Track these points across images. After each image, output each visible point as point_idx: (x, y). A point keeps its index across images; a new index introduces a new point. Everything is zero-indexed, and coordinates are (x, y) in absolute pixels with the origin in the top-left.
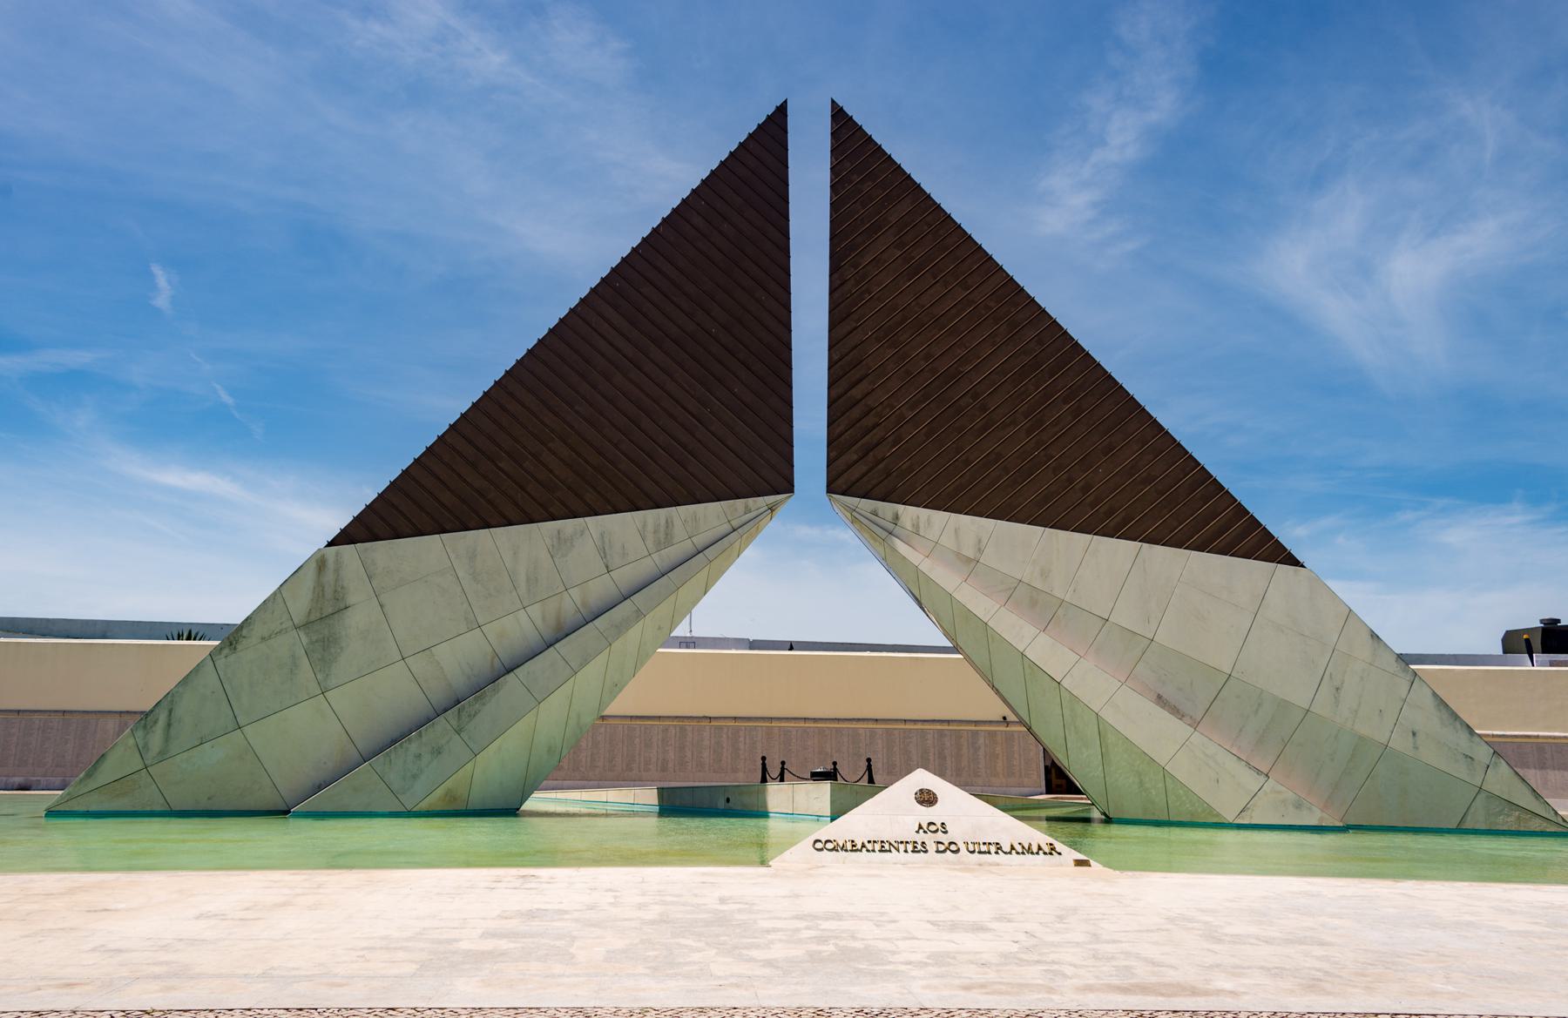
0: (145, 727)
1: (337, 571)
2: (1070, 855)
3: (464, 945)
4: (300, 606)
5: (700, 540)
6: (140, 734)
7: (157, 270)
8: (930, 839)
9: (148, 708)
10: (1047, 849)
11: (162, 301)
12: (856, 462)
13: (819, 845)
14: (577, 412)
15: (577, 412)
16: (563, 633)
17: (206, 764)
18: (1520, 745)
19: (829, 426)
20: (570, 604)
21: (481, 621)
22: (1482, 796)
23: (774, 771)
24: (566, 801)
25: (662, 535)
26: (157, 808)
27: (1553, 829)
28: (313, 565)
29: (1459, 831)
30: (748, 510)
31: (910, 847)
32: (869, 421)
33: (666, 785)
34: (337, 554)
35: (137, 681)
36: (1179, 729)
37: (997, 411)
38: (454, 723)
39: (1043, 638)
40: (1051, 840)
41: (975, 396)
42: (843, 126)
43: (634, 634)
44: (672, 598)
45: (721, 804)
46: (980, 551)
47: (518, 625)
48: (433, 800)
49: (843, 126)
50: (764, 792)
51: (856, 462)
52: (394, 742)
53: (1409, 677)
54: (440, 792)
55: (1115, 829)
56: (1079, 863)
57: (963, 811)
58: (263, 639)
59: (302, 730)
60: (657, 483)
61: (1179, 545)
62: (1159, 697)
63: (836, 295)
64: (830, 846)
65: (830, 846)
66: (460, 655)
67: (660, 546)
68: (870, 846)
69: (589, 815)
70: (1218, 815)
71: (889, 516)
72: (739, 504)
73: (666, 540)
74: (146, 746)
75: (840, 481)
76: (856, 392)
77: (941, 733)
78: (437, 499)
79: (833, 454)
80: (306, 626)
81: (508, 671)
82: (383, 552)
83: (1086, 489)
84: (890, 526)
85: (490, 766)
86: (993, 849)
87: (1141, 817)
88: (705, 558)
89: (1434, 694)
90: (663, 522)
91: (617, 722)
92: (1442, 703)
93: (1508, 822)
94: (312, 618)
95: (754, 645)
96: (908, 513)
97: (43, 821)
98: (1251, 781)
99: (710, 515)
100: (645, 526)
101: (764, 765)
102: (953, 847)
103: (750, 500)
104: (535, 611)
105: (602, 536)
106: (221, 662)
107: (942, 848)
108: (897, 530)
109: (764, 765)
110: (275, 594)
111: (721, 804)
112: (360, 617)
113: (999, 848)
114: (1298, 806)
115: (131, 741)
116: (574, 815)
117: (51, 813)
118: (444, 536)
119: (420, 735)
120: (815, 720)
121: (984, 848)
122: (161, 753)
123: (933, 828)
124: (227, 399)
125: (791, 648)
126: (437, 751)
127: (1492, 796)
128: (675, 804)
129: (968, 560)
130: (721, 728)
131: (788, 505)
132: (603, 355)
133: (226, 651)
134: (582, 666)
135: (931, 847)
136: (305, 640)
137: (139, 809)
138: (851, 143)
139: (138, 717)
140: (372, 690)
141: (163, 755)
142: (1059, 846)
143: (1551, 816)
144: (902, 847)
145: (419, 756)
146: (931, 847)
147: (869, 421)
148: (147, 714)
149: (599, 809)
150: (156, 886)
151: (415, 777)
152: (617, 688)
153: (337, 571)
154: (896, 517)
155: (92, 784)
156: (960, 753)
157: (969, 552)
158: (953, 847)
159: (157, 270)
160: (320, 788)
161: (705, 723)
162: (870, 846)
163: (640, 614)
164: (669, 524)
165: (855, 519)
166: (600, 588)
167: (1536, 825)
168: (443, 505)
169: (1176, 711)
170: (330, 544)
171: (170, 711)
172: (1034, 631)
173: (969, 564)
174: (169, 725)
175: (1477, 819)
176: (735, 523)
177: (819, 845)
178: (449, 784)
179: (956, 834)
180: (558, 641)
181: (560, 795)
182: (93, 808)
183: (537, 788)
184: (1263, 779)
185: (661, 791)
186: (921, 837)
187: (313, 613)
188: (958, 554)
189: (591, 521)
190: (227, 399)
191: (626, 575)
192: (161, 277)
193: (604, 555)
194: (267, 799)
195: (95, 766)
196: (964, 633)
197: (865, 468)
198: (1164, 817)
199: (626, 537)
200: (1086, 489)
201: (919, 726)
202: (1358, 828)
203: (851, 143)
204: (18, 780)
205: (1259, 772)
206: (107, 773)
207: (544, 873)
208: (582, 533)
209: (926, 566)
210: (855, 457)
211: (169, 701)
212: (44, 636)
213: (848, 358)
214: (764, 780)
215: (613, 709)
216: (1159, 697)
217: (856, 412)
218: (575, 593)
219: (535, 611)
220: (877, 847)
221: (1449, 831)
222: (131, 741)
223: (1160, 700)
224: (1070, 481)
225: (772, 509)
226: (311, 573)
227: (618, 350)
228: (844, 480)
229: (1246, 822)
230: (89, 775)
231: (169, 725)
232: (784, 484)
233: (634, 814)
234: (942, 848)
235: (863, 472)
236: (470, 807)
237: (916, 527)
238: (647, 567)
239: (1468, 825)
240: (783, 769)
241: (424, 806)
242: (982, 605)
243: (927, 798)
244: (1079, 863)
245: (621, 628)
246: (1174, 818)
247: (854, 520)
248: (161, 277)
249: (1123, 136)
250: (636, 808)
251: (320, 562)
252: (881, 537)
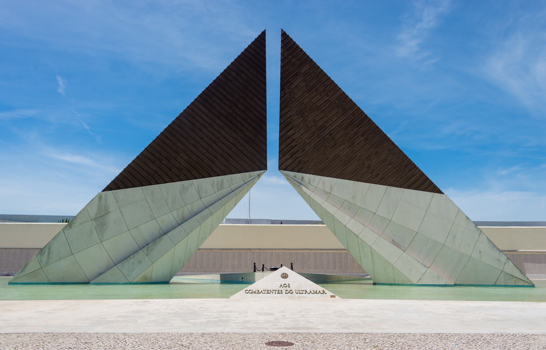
0: (41, 254)
1: (106, 200)
2: (329, 294)
3: (108, 319)
4: (93, 213)
5: (233, 187)
6: (39, 256)
7: (58, 78)
8: (284, 289)
9: (43, 247)
10: (322, 292)
11: (61, 90)
12: (288, 159)
13: (247, 292)
14: (189, 143)
15: (189, 143)
16: (184, 220)
17: (61, 267)
18: (533, 255)
19: (279, 146)
20: (187, 211)
21: (156, 216)
22: (503, 273)
23: (259, 267)
24: (190, 279)
25: (220, 186)
26: (45, 282)
27: (527, 284)
28: (97, 198)
29: (495, 285)
30: (250, 176)
31: (277, 292)
32: (294, 144)
33: (222, 273)
34: (106, 194)
35: (37, 237)
36: (399, 251)
37: (340, 139)
38: (146, 252)
39: (353, 220)
40: (323, 289)
41: (331, 135)
42: (286, 39)
43: (209, 220)
44: (223, 207)
45: (240, 280)
46: (332, 190)
47: (168, 218)
48: (139, 279)
49: (286, 39)
50: (254, 275)
51: (288, 159)
52: (126, 259)
53: (479, 232)
54: (141, 276)
55: (377, 287)
56: (332, 296)
57: (296, 280)
58: (81, 224)
59: (93, 257)
60: (218, 167)
61: (401, 187)
62: (393, 240)
63: (282, 99)
64: (250, 292)
65: (250, 292)
66: (148, 229)
67: (219, 190)
68: (264, 292)
69: (199, 284)
70: (411, 282)
71: (300, 178)
72: (247, 174)
73: (222, 187)
74: (41, 261)
75: (283, 166)
76: (289, 134)
77: (334, 254)
78: (140, 174)
79: (281, 156)
80: (95, 219)
81: (165, 234)
82: (122, 193)
83: (369, 167)
84: (300, 181)
85: (158, 268)
86: (304, 292)
87: (385, 282)
88: (236, 193)
89: (488, 238)
90: (220, 181)
91: (217, 251)
92: (490, 241)
93: (511, 282)
94: (97, 216)
95: (273, 222)
96: (307, 177)
97: (8, 286)
98: (423, 270)
99: (237, 178)
100: (213, 182)
101: (255, 266)
102: (291, 292)
103: (251, 173)
104: (175, 213)
105: (198, 186)
106: (66, 232)
107: (287, 292)
108: (303, 183)
109: (255, 266)
110: (84, 208)
111: (240, 280)
112: (114, 216)
113: (306, 292)
114: (438, 278)
115: (36, 259)
116: (196, 284)
117: (10, 283)
118: (143, 187)
119: (134, 256)
120: (288, 249)
121: (301, 292)
122: (46, 263)
123: (285, 286)
124: (87, 127)
125: (281, 223)
126: (140, 262)
127: (506, 273)
128: (226, 280)
129: (327, 193)
130: (254, 253)
131: (267, 172)
132: (199, 122)
133: (68, 228)
134: (191, 232)
135: (284, 292)
136: (95, 224)
137: (39, 282)
138: (288, 45)
139: (37, 252)
140: (119, 242)
141: (47, 264)
142: (326, 291)
143: (526, 280)
144: (274, 292)
145: (133, 264)
146: (284, 292)
147: (294, 144)
148: (42, 250)
149: (202, 282)
150: (29, 304)
151: (132, 271)
152: (204, 239)
153: (106, 200)
154: (303, 178)
155: (24, 274)
156: (295, 260)
157: (328, 190)
158: (291, 292)
159: (58, 78)
160: (100, 275)
161: (248, 251)
162: (264, 292)
163: (211, 214)
164: (222, 181)
165: (288, 178)
166: (198, 204)
167: (521, 283)
168: (143, 177)
169: (398, 246)
170: (103, 191)
171: (49, 249)
172: (349, 218)
173: (328, 194)
174: (49, 253)
175: (501, 282)
176: (246, 181)
177: (247, 292)
178: (144, 273)
179: (293, 287)
180: (182, 223)
181: (189, 277)
182: (24, 282)
183: (175, 274)
184: (426, 268)
185: (221, 275)
186: (280, 289)
187: (98, 216)
188: (324, 191)
189: (194, 181)
190: (87, 127)
191: (207, 200)
192: (60, 81)
193: (199, 192)
194: (82, 278)
195: (25, 267)
196: (325, 218)
197: (292, 161)
198: (393, 282)
199: (207, 185)
200: (369, 167)
201: (326, 251)
202: (460, 285)
203: (287, 42)
204: (5, 273)
205: (425, 266)
206: (29, 269)
207: (152, 301)
208: (191, 185)
209: (312, 195)
210: (289, 157)
211: (49, 246)
212: (15, 221)
213: (286, 122)
214: (255, 271)
215: (204, 246)
216: (393, 240)
217: (289, 141)
218: (189, 206)
219: (175, 213)
220: (266, 292)
221: (492, 286)
222: (36, 259)
223: (393, 242)
224: (363, 164)
225: (259, 176)
226: (97, 201)
227: (204, 120)
228: (285, 165)
229: (420, 283)
230: (22, 271)
231: (49, 253)
232: (263, 166)
233: (213, 283)
234: (287, 292)
235: (291, 163)
236: (152, 281)
237: (310, 181)
238: (214, 197)
239: (498, 284)
240: (263, 267)
241: (135, 281)
242: (331, 209)
243: (285, 276)
244: (332, 296)
245: (204, 219)
246: (397, 283)
247: (288, 179)
248: (60, 81)
249: (429, 18)
250: (213, 281)
251: (100, 197)
252: (298, 185)
